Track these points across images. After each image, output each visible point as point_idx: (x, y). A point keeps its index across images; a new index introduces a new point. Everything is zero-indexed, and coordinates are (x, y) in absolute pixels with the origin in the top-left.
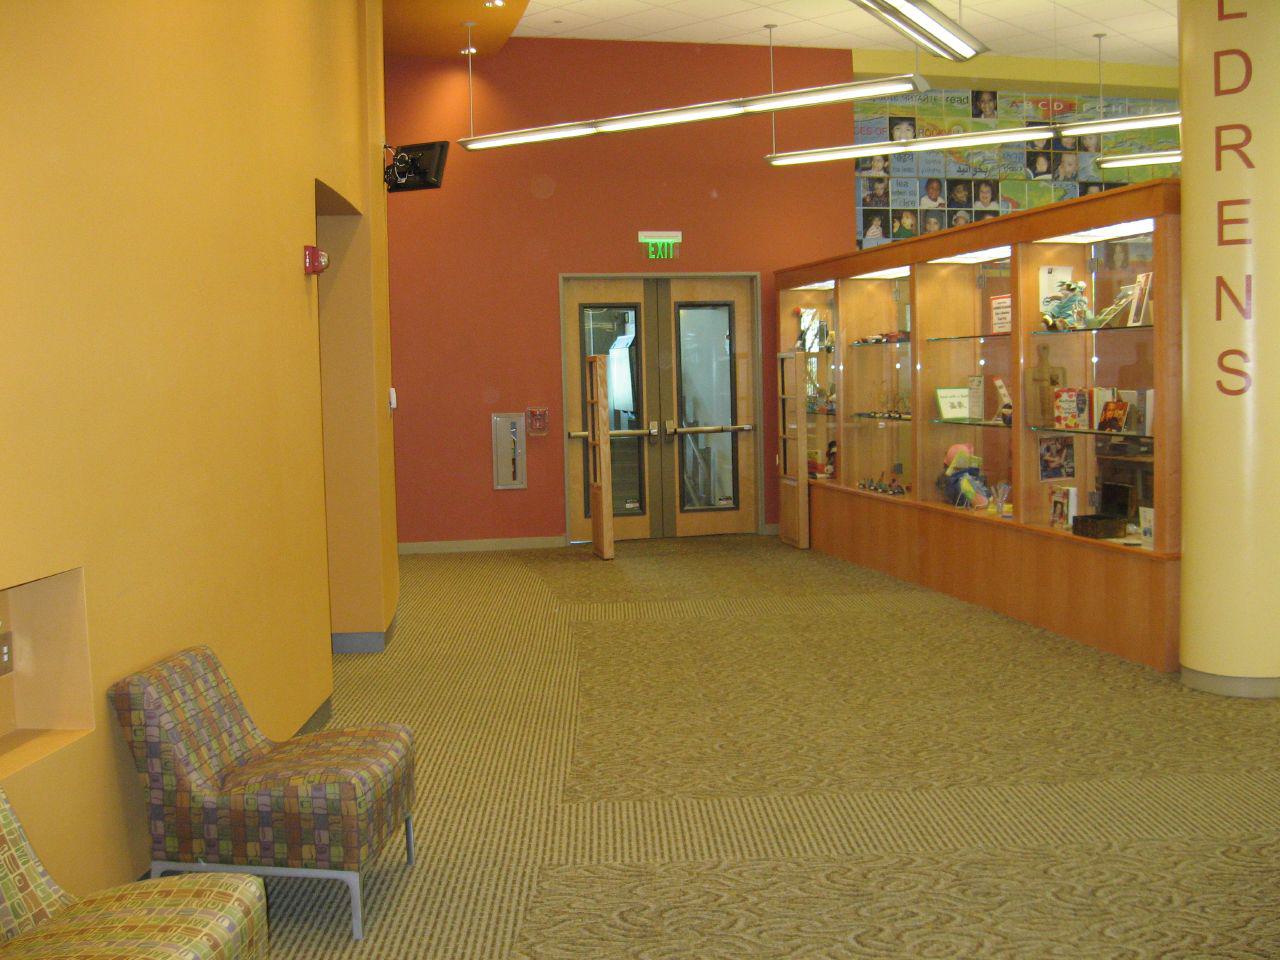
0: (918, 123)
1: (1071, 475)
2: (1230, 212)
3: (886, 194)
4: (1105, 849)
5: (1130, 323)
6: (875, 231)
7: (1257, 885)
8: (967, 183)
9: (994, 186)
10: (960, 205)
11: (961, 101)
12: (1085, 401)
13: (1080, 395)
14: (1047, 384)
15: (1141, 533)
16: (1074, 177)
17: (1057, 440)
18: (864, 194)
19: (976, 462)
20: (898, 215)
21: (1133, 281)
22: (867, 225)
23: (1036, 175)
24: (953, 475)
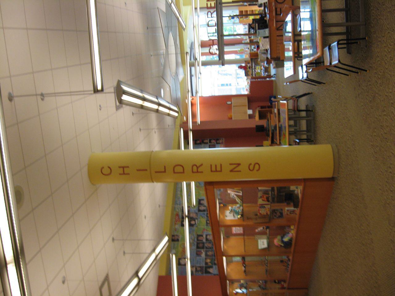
0: (180, 257)
1: (282, 210)
2: (214, 169)
3: (200, 267)
4: (381, 190)
5: (241, 194)
6: (211, 270)
7: (384, 152)
8: (198, 244)
9: (199, 236)
10: (204, 245)
11: (174, 245)
12: (262, 206)
13: (260, 207)
14: (257, 217)
15: (298, 190)
16: (197, 213)
17: (272, 214)
18: (200, 273)
19: (279, 237)
20: (206, 263)
21: (229, 194)
22: (209, 273)
23: (196, 224)
24: (284, 244)
